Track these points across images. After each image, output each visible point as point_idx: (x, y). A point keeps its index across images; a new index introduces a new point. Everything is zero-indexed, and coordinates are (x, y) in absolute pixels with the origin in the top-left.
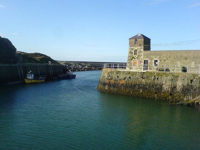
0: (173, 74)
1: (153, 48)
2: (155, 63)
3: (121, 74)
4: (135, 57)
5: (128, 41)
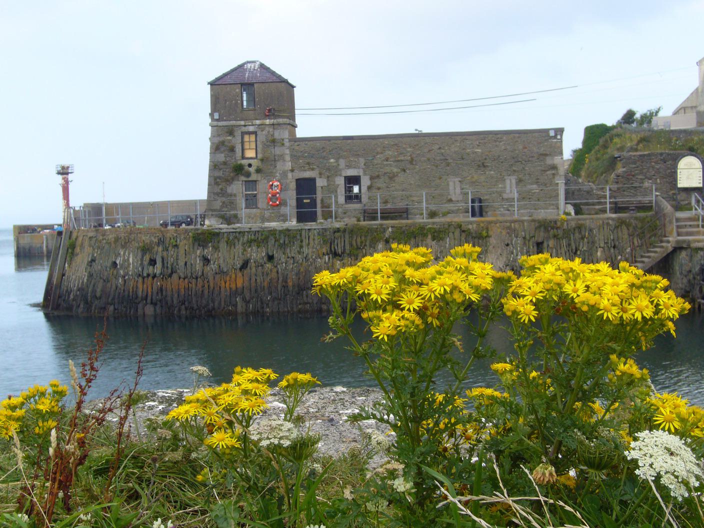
0: (464, 227)
3: (223, 245)
5: (207, 91)
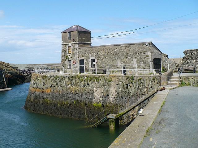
1: (95, 42)
2: (92, 63)
4: (69, 56)
